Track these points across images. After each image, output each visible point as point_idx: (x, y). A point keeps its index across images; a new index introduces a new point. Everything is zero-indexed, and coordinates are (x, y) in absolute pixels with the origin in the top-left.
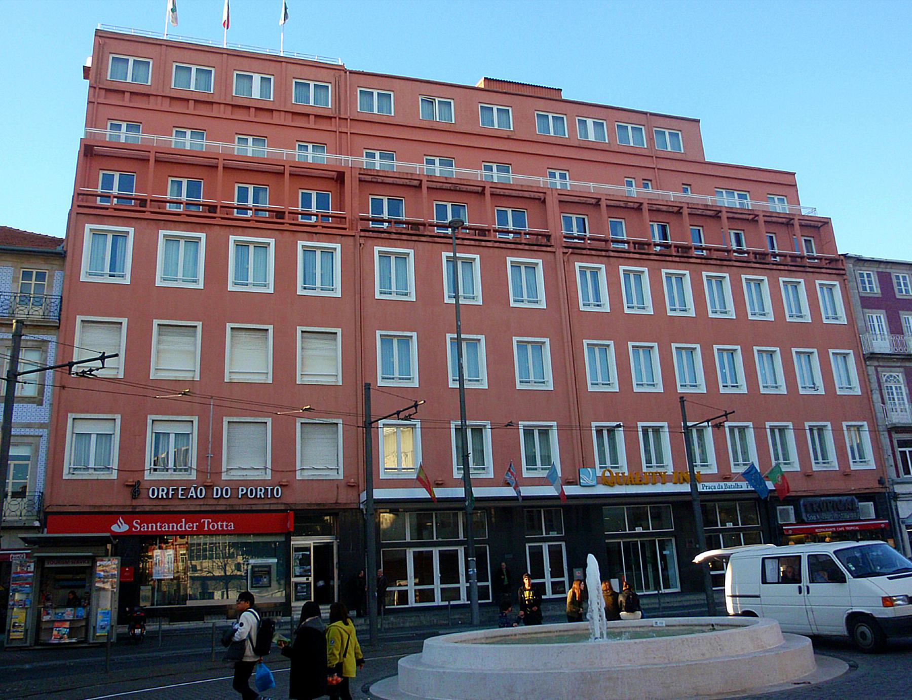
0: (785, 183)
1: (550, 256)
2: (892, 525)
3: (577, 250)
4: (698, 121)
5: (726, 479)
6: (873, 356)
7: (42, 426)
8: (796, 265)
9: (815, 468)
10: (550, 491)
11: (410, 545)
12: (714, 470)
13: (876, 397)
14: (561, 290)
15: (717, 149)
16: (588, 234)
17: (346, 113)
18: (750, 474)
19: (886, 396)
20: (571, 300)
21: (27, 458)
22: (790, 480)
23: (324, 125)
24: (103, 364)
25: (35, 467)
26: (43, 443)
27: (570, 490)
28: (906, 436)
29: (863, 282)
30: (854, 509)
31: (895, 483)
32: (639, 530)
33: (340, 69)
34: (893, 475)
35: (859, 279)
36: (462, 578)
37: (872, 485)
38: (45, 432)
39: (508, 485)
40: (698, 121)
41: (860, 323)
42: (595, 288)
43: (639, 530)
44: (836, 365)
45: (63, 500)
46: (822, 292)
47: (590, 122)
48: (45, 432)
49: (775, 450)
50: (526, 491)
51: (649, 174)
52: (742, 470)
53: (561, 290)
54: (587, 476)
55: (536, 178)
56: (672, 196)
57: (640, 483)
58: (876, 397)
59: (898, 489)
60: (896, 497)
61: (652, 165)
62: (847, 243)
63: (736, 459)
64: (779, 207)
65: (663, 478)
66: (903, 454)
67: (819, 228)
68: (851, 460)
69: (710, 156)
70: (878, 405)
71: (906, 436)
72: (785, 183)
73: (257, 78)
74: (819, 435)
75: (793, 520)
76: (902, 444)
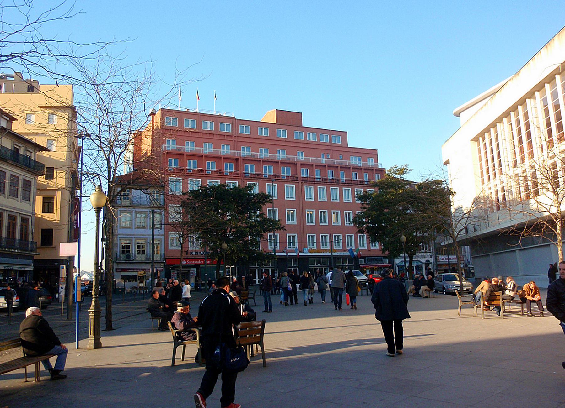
0: (373, 153)
1: (297, 184)
2: (393, 265)
3: (306, 181)
5: (345, 251)
7: (162, 235)
10: (295, 254)
11: (257, 268)
12: (329, 248)
14: (300, 194)
15: (352, 143)
16: (290, 175)
18: (351, 251)
20: (303, 197)
21: (144, 244)
23: (229, 139)
25: (161, 246)
26: (163, 239)
27: (300, 254)
30: (381, 260)
32: (319, 265)
33: (234, 118)
36: (257, 277)
38: (163, 237)
39: (284, 252)
42: (309, 193)
43: (319, 265)
44: (334, 217)
45: (169, 255)
46: (333, 192)
47: (311, 134)
48: (163, 237)
49: (348, 243)
50: (289, 254)
52: (349, 248)
53: (300, 194)
54: (305, 250)
57: (320, 252)
61: (330, 149)
63: (348, 245)
64: (370, 163)
65: (326, 251)
72: (373, 153)
73: (209, 122)
74: (14, 233)
75: (363, 263)
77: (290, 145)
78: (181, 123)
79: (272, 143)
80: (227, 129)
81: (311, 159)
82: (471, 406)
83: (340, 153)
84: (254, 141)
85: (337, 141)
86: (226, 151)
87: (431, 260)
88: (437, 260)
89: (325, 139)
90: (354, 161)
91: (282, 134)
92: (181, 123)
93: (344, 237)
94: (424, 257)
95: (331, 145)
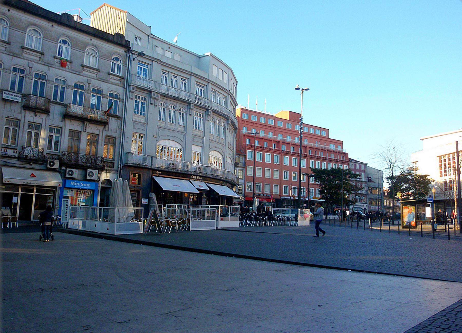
0: (340, 143)
15: (332, 136)
33: (275, 117)
64: (339, 148)
72: (340, 143)
77: (293, 133)
78: (250, 117)
79: (285, 131)
80: (271, 123)
81: (312, 145)
82: (219, 315)
83: (326, 142)
84: (275, 129)
85: (324, 134)
86: (270, 136)
87: (367, 208)
88: (369, 208)
89: (318, 133)
90: (332, 147)
91: (290, 126)
92: (250, 117)
93: (315, 190)
94: (363, 206)
95: (321, 136)
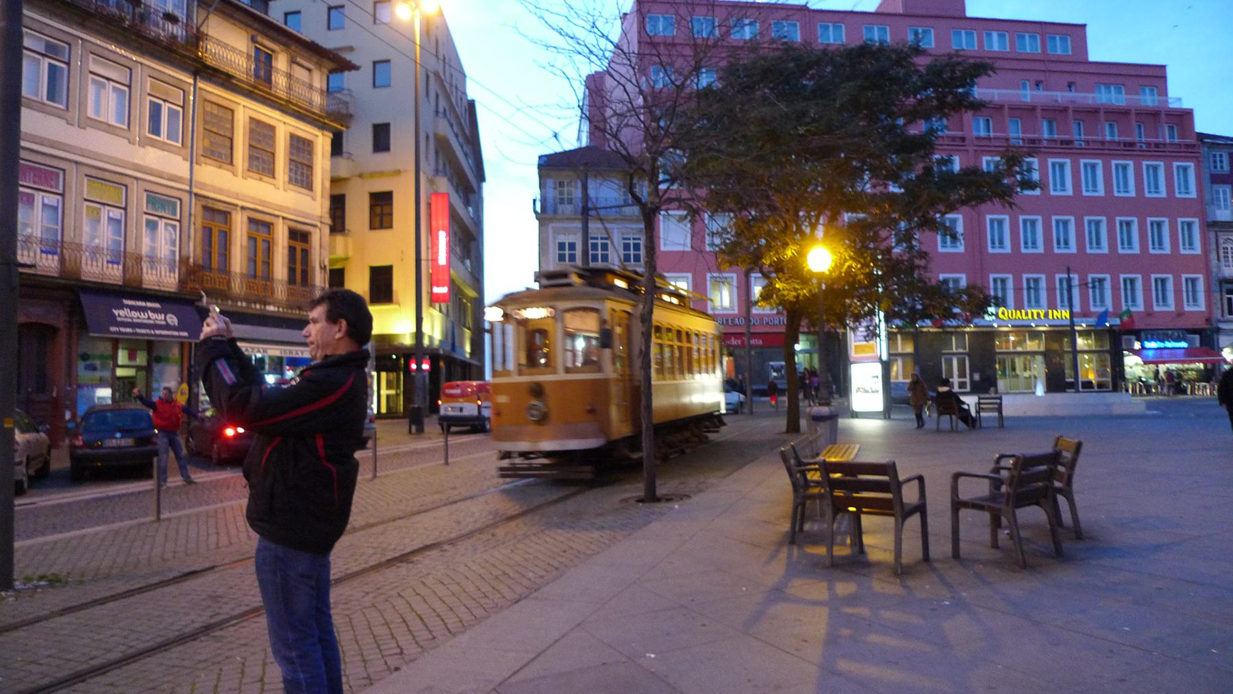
4: (1084, 26)
6: (1215, 224)
8: (1158, 150)
9: (1156, 309)
13: (1213, 256)
17: (97, 111)
19: (1222, 255)
22: (1136, 318)
24: (974, 505)
28: (1230, 286)
29: (1215, 162)
31: (1219, 321)
34: (1219, 316)
35: (1211, 160)
37: (1201, 324)
40: (1084, 26)
41: (1207, 197)
51: (1041, 77)
55: (991, 91)
56: (1061, 96)
58: (1213, 256)
59: (1222, 326)
60: (1218, 330)
62: (1203, 124)
64: (1148, 100)
66: (1230, 299)
67: (1185, 116)
68: (1022, 245)
69: (1093, 57)
70: (1214, 261)
71: (1230, 286)
72: (1155, 76)
76: (1230, 292)
